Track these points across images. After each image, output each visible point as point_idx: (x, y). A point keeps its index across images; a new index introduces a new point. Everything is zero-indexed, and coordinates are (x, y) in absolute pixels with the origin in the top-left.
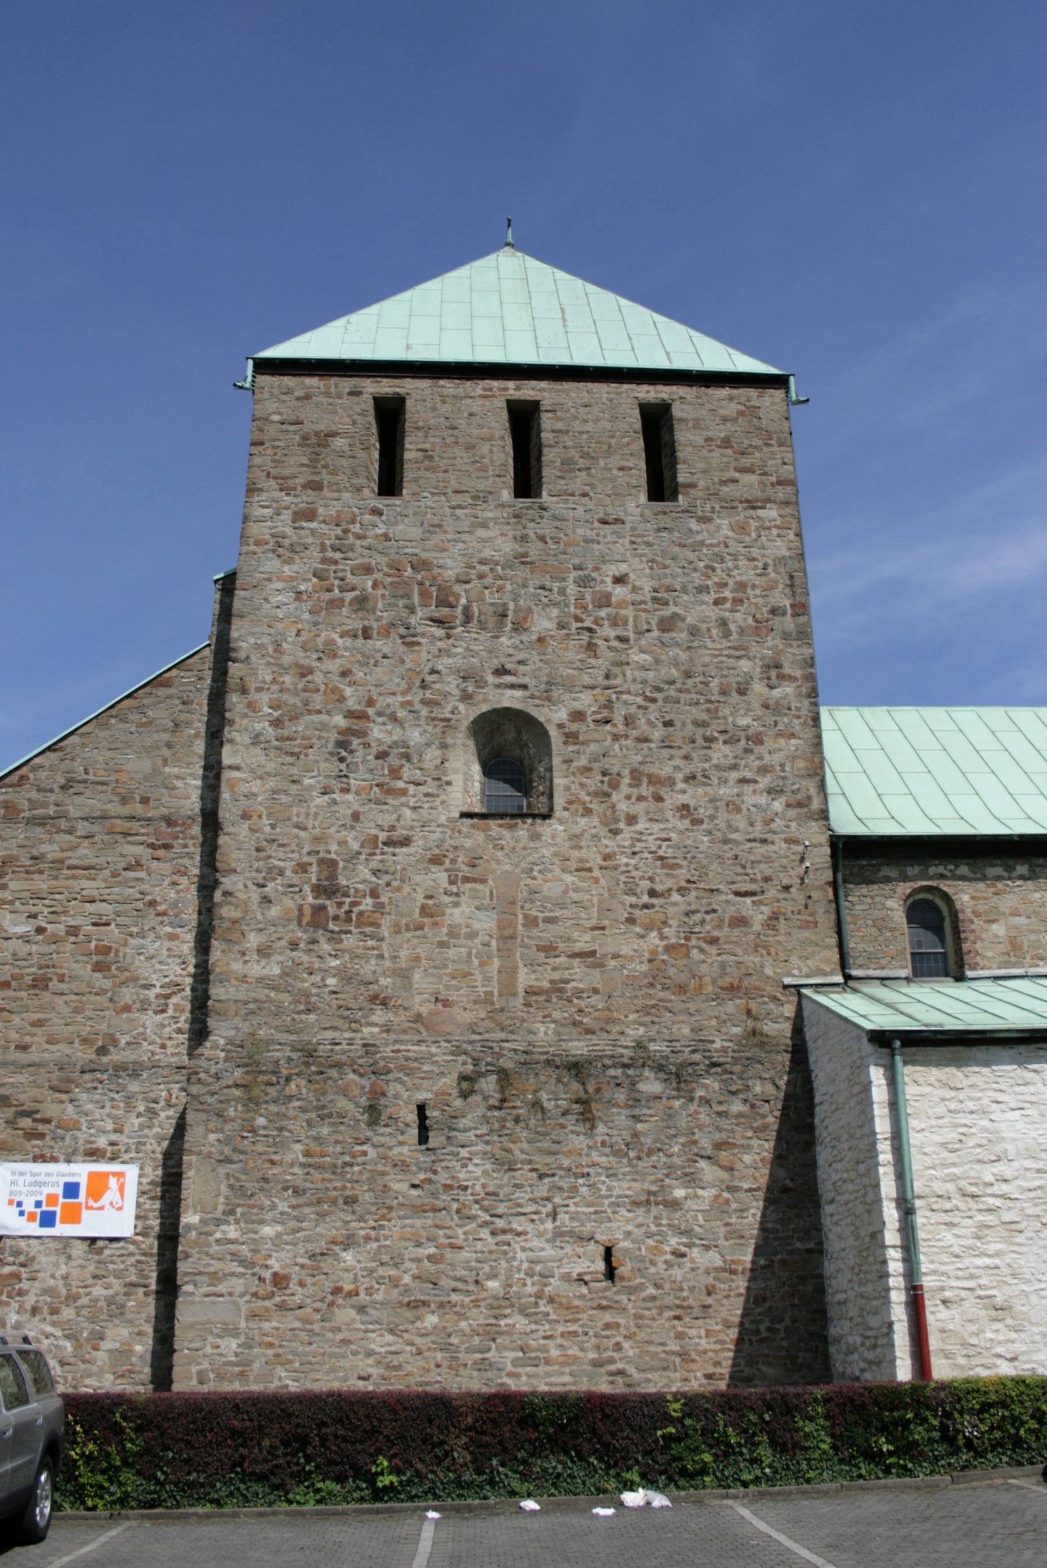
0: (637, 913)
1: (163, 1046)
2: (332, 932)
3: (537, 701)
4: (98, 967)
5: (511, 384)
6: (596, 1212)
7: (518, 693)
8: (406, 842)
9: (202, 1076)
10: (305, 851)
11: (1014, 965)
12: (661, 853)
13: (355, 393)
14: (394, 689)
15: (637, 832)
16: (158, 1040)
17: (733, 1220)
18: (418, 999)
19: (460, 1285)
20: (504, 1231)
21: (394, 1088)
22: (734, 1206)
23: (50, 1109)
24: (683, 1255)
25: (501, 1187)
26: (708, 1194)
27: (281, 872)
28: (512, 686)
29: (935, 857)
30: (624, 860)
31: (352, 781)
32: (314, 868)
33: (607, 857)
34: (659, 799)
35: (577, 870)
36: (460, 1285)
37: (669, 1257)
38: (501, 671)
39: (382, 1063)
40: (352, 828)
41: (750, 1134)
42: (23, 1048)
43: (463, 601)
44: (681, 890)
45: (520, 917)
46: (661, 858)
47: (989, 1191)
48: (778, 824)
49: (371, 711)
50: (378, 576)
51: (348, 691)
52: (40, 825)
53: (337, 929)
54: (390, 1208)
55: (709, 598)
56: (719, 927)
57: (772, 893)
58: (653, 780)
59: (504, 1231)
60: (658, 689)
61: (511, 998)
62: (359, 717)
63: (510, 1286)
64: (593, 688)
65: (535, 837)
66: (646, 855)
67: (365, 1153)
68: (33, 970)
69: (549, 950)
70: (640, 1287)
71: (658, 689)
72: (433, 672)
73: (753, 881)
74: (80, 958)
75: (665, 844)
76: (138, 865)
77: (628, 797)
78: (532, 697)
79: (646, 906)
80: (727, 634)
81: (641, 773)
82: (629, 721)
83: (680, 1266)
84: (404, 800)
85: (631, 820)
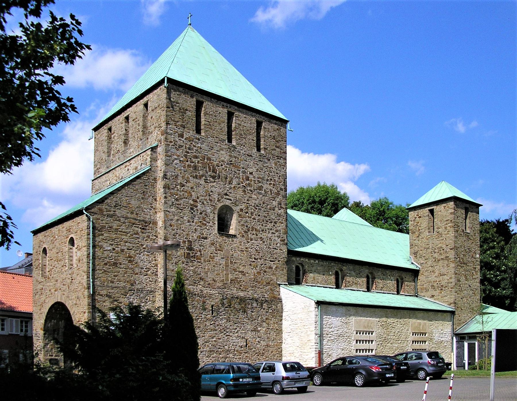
2: (191, 260)
3: (233, 205)
4: (130, 261)
6: (245, 332)
7: (230, 202)
8: (206, 238)
10: (184, 238)
11: (314, 283)
12: (257, 249)
14: (203, 195)
15: (252, 243)
16: (145, 283)
17: (268, 335)
18: (209, 280)
19: (220, 347)
20: (228, 336)
22: (269, 332)
24: (259, 342)
25: (227, 325)
26: (264, 329)
28: (228, 199)
29: (303, 257)
30: (250, 250)
31: (195, 220)
35: (241, 251)
36: (220, 347)
37: (257, 342)
38: (226, 194)
39: (204, 295)
40: (195, 233)
41: (272, 317)
42: (112, 282)
43: (218, 172)
44: (260, 259)
45: (230, 261)
46: (257, 250)
47: (330, 333)
48: (278, 245)
49: (198, 200)
50: (199, 160)
51: (193, 193)
52: (111, 217)
53: (192, 259)
56: (266, 269)
58: (256, 230)
59: (228, 336)
61: (228, 281)
62: (195, 202)
63: (229, 347)
64: (245, 203)
65: (233, 241)
66: (254, 249)
68: (113, 260)
69: (235, 270)
72: (212, 192)
73: (273, 258)
74: (125, 258)
75: (258, 246)
76: (137, 233)
77: (251, 234)
78: (232, 203)
79: (253, 262)
81: (254, 228)
82: (252, 213)
83: (259, 344)
84: (205, 227)
85: (251, 240)
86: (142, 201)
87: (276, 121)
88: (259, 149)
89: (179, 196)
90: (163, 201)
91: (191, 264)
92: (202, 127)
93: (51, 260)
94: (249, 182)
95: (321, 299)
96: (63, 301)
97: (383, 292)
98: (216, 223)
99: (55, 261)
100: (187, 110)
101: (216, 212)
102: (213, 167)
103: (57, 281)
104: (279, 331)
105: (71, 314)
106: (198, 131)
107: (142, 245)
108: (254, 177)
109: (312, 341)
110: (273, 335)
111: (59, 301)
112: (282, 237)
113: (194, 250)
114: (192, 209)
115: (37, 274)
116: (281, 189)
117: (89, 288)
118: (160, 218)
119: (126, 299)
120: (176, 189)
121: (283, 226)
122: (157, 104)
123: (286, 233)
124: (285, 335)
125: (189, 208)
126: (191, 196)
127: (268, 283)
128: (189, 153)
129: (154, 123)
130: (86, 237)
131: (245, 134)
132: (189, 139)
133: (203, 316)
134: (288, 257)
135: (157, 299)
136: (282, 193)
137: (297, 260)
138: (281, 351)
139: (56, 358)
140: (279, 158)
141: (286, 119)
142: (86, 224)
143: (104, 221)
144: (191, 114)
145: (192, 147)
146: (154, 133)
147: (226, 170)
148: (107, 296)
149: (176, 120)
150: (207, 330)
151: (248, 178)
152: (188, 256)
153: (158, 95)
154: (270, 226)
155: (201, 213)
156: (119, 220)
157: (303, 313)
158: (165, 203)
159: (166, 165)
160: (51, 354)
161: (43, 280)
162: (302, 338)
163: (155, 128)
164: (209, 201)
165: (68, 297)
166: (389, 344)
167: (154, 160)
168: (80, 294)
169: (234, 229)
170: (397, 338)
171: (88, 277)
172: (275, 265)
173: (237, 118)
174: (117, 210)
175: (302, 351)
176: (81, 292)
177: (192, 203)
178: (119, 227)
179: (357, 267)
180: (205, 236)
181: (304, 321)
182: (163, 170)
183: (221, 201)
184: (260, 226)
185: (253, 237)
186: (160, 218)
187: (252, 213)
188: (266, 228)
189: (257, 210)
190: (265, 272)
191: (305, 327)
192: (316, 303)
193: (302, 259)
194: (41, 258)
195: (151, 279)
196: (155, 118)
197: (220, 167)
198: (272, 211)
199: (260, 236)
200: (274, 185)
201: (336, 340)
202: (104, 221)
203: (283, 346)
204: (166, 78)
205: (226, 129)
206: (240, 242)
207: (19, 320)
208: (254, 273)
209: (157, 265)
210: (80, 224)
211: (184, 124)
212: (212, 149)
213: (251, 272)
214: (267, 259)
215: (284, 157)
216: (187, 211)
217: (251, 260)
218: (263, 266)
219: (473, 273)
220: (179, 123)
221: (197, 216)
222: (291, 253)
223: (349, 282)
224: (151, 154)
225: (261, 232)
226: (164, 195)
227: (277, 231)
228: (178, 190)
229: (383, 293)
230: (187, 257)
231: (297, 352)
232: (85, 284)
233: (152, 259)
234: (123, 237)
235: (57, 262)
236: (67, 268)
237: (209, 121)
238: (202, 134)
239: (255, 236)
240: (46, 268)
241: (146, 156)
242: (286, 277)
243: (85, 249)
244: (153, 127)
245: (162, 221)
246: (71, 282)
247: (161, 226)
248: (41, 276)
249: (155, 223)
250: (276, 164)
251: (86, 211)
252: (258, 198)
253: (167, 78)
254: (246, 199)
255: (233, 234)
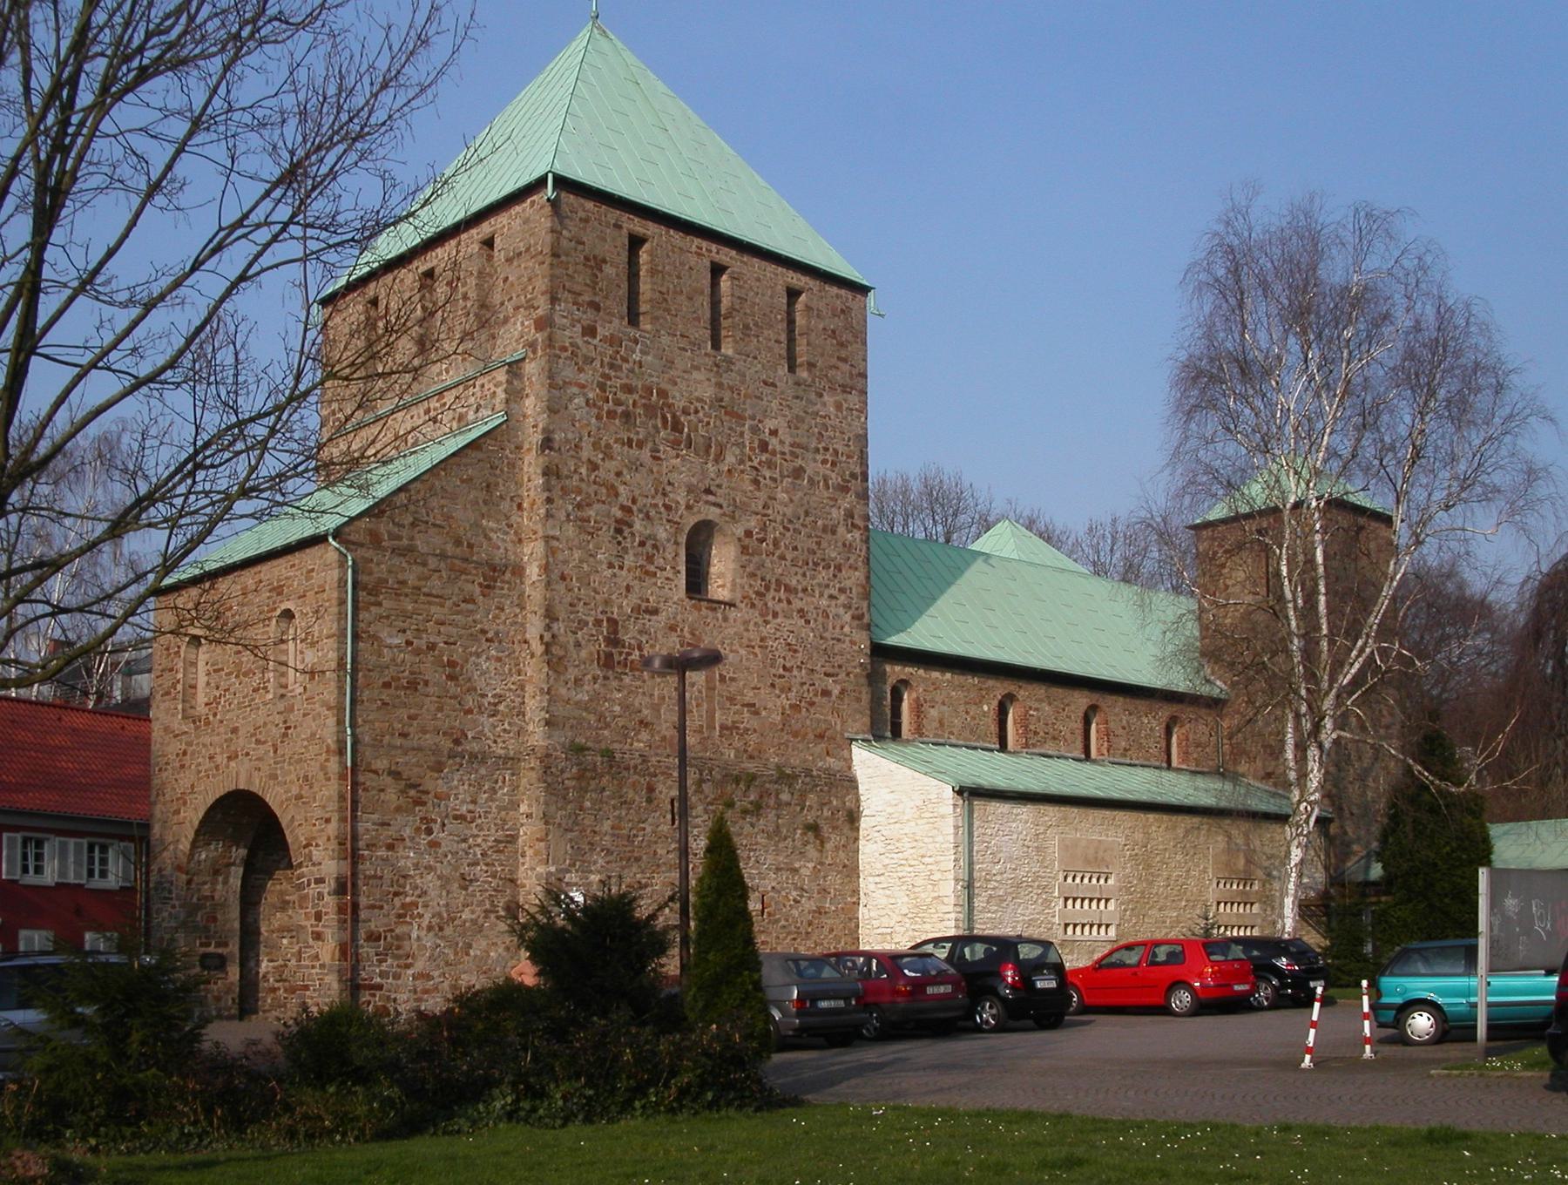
0: (777, 680)
1: (495, 742)
4: (451, 677)
5: (714, 247)
7: (718, 511)
8: (655, 612)
9: (553, 770)
13: (618, 226)
21: (660, 787)
23: (428, 784)
26: (811, 865)
27: (586, 624)
32: (605, 624)
33: (762, 640)
34: (789, 602)
38: (708, 491)
39: (652, 770)
42: (404, 735)
49: (635, 508)
50: (636, 397)
51: (621, 489)
52: (400, 555)
54: (658, 866)
55: (819, 457)
56: (816, 695)
57: (842, 676)
58: (788, 589)
60: (790, 521)
64: (757, 514)
67: (644, 829)
69: (731, 700)
70: (778, 921)
71: (790, 521)
72: (670, 483)
76: (470, 600)
78: (724, 514)
79: (781, 676)
80: (827, 487)
82: (776, 543)
84: (654, 580)
85: (775, 615)
86: (484, 509)
87: (839, 287)
88: (792, 369)
89: (584, 496)
90: (542, 511)
91: (615, 684)
92: (643, 308)
93: (215, 671)
94: (767, 455)
95: (969, 781)
96: (254, 789)
97: (1128, 761)
98: (683, 568)
99: (230, 674)
100: (604, 261)
101: (683, 539)
102: (674, 416)
103: (235, 730)
104: (851, 871)
105: (284, 825)
106: (633, 318)
107: (484, 632)
108: (782, 442)
109: (946, 900)
110: (834, 880)
111: (241, 787)
112: (857, 609)
113: (624, 647)
114: (619, 531)
115: (167, 711)
116: (853, 476)
117: (341, 752)
118: (532, 556)
119: (440, 781)
120: (576, 477)
121: (859, 575)
122: (522, 244)
123: (866, 596)
124: (866, 884)
125: (612, 530)
126: (617, 495)
127: (821, 736)
128: (610, 379)
129: (514, 295)
130: (335, 610)
131: (756, 324)
132: (612, 341)
133: (649, 829)
134: (872, 663)
135: (524, 781)
136: (855, 485)
137: (895, 671)
138: (857, 926)
139: (220, 951)
140: (846, 389)
141: (865, 282)
142: (335, 574)
143: (382, 566)
144: (614, 271)
145: (619, 362)
146: (515, 324)
147: (708, 423)
148: (390, 773)
149: (577, 288)
150: (658, 866)
151: (764, 446)
152: (607, 662)
153: (527, 221)
154: (823, 575)
155: (642, 544)
156: (424, 564)
157: (920, 822)
158: (549, 515)
159: (552, 410)
160: (204, 940)
161: (188, 727)
162: (916, 890)
163: (517, 308)
164: (662, 509)
165: (274, 777)
166: (1153, 912)
167: (514, 395)
168: (313, 769)
169: (728, 585)
170: (1175, 892)
171: (340, 722)
172: (839, 687)
173: (736, 282)
174: (417, 536)
175: (917, 927)
176: (318, 764)
177: (619, 514)
178: (423, 583)
179: (1058, 692)
180: (652, 604)
181: (921, 844)
182: (541, 426)
183: (695, 509)
184: (799, 577)
185: (778, 608)
186: (532, 556)
187: (776, 543)
188: (814, 582)
189: (788, 534)
190: (812, 704)
191: (926, 860)
192: (960, 792)
193: (907, 669)
194: (181, 664)
195: (506, 726)
196: (516, 283)
197: (692, 417)
198: (829, 536)
199: (797, 604)
200: (834, 464)
201: (1010, 898)
202: (382, 566)
203: (862, 912)
204: (550, 175)
205: (708, 315)
206: (746, 623)
207: (85, 842)
208: (783, 708)
209: (522, 688)
210: (314, 574)
211: (597, 299)
212: (670, 368)
213: (774, 705)
214: (818, 668)
215: (859, 386)
216: (606, 534)
217: (773, 671)
218: (805, 687)
219: (1380, 711)
220: (586, 298)
221: (631, 552)
222: (883, 653)
223: (1036, 733)
224: (509, 382)
225: (800, 595)
226: (546, 494)
227: (842, 590)
228: (582, 480)
229: (1130, 765)
230: (605, 665)
231: (903, 929)
232: (331, 741)
233: (510, 670)
234: (434, 609)
235: (237, 677)
236: (270, 696)
237: (664, 290)
238: (642, 327)
239: (784, 604)
240: (195, 694)
241: (491, 385)
242: (867, 720)
243: (331, 643)
244: (509, 306)
245: (540, 567)
246: (285, 735)
247: (535, 578)
248: (180, 716)
249: (519, 571)
250: (839, 407)
251: (334, 539)
252: (791, 501)
253: (554, 174)
254: (760, 504)
255: (726, 599)
